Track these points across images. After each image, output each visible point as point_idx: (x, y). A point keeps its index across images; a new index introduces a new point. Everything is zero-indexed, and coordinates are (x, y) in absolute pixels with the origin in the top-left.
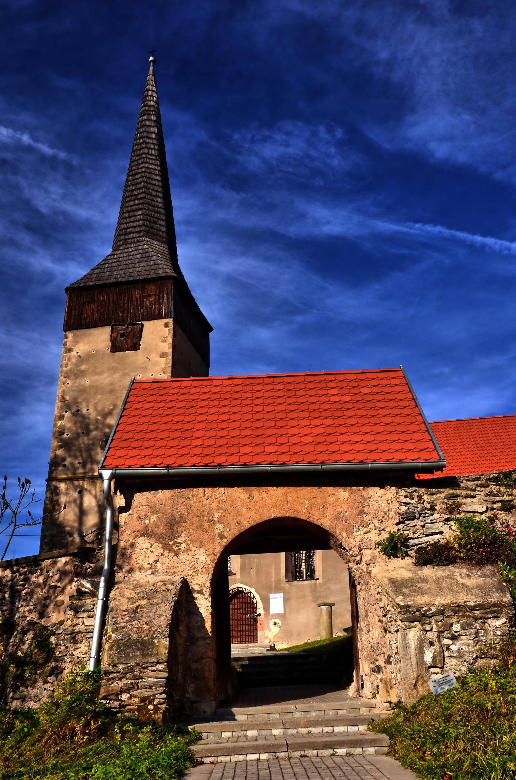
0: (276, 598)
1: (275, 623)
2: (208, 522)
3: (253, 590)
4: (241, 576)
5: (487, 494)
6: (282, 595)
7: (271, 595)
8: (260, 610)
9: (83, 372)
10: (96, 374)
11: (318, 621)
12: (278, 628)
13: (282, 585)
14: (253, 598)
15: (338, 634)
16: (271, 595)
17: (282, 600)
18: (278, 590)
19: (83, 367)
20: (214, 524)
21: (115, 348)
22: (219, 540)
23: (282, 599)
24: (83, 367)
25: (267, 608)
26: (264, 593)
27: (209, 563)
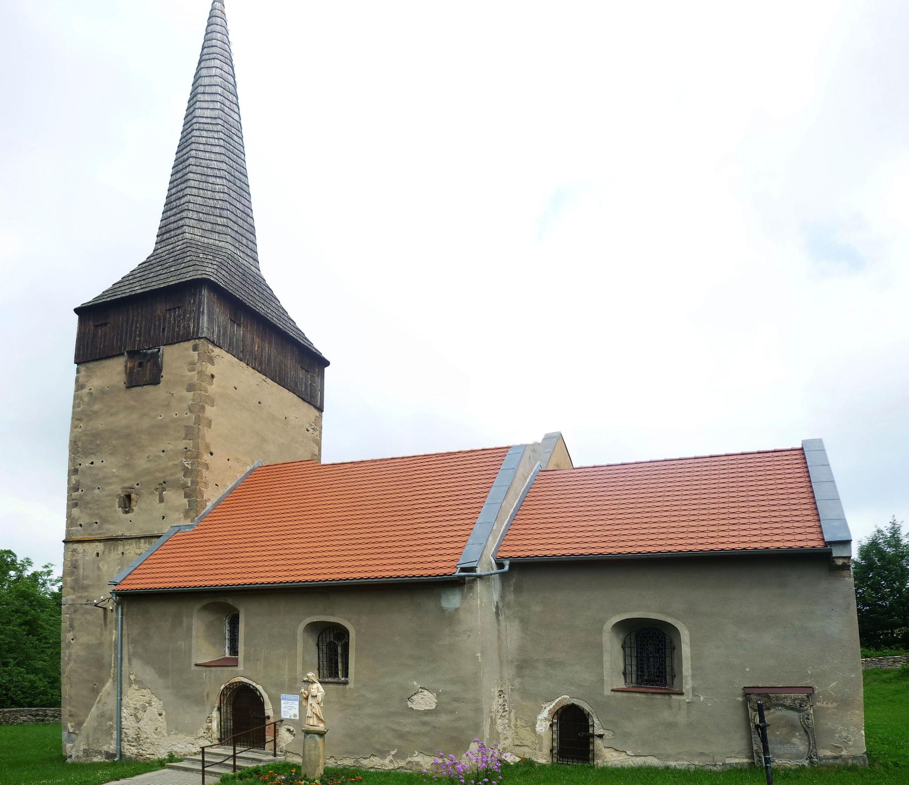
3: (259, 687)
7: (283, 696)
8: (269, 711)
9: (96, 413)
10: (111, 415)
17: (297, 703)
19: (96, 407)
21: (133, 381)
24: (96, 407)
25: (277, 711)
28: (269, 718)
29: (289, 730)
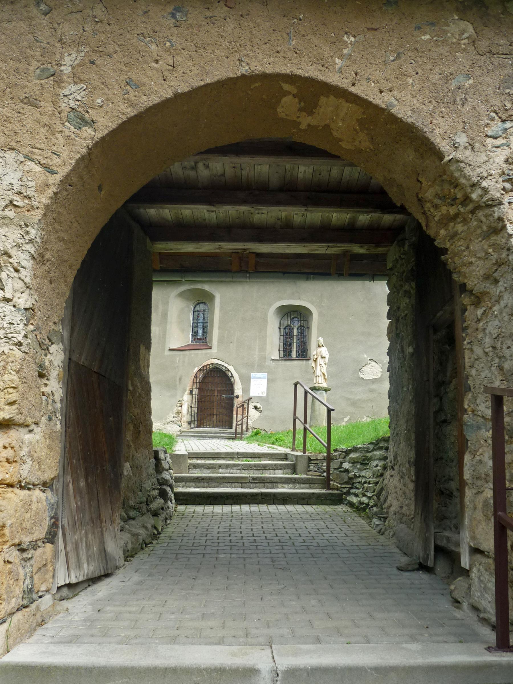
0: (258, 378)
1: (256, 408)
2: (39, 78)
3: (231, 368)
4: (218, 350)
5: (5, 527)
6: (266, 375)
7: (253, 375)
8: (238, 391)
11: (142, 644)
12: (259, 412)
13: (267, 364)
14: (231, 377)
15: (490, 396)
16: (253, 375)
17: (265, 381)
18: (261, 369)
20: (59, 83)
22: (70, 129)
23: (266, 380)
25: (246, 389)
26: (244, 371)
27: (30, 192)
28: (237, 397)
29: (256, 408)
